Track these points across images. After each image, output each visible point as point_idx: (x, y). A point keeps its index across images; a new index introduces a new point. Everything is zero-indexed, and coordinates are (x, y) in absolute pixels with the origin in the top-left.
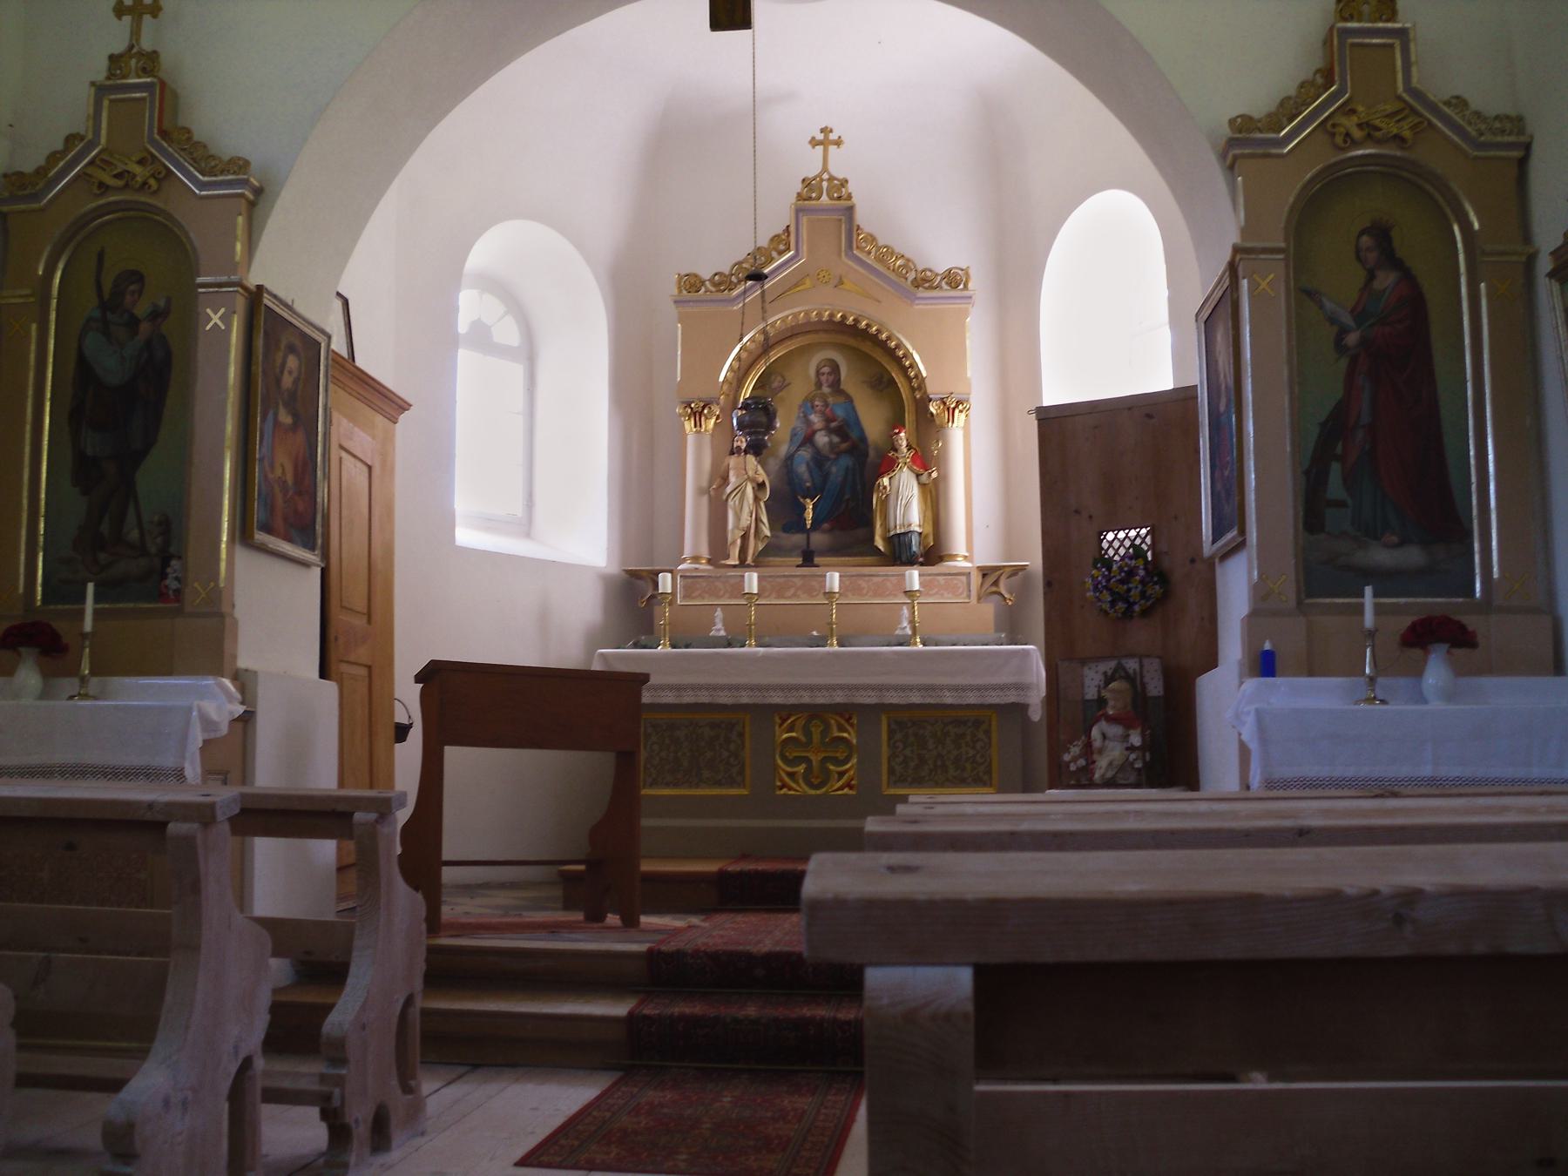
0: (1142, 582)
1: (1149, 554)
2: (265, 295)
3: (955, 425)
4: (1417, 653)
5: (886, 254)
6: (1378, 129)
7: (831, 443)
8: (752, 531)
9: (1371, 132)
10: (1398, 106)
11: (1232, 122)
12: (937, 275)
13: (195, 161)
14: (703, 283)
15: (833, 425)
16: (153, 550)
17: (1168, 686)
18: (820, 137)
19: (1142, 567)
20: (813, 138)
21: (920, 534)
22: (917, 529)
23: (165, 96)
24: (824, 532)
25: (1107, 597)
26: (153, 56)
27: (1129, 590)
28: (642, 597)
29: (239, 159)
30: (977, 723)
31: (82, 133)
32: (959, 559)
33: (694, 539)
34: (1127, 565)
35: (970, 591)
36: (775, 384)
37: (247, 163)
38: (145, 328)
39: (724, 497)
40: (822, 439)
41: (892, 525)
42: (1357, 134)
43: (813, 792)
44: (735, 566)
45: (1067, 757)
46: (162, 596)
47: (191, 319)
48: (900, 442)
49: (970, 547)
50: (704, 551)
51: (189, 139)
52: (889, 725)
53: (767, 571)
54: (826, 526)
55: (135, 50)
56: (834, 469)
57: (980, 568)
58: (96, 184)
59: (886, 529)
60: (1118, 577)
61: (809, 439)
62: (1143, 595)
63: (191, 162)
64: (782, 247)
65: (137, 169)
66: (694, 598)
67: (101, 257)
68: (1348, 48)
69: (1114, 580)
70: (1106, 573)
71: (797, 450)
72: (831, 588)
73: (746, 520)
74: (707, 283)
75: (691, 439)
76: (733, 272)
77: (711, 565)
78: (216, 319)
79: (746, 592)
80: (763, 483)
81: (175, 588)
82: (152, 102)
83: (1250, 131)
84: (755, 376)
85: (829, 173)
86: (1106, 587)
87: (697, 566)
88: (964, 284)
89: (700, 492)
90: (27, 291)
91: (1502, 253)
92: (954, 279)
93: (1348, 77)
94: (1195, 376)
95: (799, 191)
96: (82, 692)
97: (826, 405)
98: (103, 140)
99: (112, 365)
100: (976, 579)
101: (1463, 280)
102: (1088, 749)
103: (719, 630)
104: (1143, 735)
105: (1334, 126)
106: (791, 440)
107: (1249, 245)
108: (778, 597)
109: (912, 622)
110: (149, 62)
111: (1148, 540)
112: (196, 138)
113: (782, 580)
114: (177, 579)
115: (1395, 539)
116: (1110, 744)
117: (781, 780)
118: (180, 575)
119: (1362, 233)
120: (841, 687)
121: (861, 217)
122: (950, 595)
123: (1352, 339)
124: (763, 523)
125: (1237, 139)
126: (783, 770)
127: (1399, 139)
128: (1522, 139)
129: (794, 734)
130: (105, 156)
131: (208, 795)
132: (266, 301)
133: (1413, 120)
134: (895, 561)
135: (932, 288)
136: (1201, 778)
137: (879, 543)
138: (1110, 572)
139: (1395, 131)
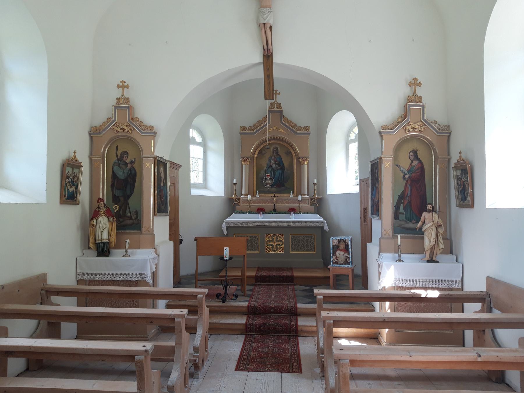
5: (290, 122)
7: (276, 166)
9: (414, 129)
12: (302, 128)
14: (246, 129)
15: (277, 163)
16: (134, 218)
24: (275, 188)
36: (263, 153)
38: (129, 166)
40: (274, 166)
43: (274, 252)
47: (141, 166)
49: (308, 193)
51: (138, 121)
52: (291, 237)
56: (277, 173)
63: (139, 126)
67: (117, 147)
78: (148, 165)
85: (277, 102)
90: (100, 156)
97: (275, 158)
101: (433, 163)
105: (406, 128)
112: (140, 120)
117: (267, 249)
119: (410, 152)
121: (284, 113)
123: (407, 176)
128: (449, 131)
130: (117, 124)
131: (181, 311)
139: (420, 129)
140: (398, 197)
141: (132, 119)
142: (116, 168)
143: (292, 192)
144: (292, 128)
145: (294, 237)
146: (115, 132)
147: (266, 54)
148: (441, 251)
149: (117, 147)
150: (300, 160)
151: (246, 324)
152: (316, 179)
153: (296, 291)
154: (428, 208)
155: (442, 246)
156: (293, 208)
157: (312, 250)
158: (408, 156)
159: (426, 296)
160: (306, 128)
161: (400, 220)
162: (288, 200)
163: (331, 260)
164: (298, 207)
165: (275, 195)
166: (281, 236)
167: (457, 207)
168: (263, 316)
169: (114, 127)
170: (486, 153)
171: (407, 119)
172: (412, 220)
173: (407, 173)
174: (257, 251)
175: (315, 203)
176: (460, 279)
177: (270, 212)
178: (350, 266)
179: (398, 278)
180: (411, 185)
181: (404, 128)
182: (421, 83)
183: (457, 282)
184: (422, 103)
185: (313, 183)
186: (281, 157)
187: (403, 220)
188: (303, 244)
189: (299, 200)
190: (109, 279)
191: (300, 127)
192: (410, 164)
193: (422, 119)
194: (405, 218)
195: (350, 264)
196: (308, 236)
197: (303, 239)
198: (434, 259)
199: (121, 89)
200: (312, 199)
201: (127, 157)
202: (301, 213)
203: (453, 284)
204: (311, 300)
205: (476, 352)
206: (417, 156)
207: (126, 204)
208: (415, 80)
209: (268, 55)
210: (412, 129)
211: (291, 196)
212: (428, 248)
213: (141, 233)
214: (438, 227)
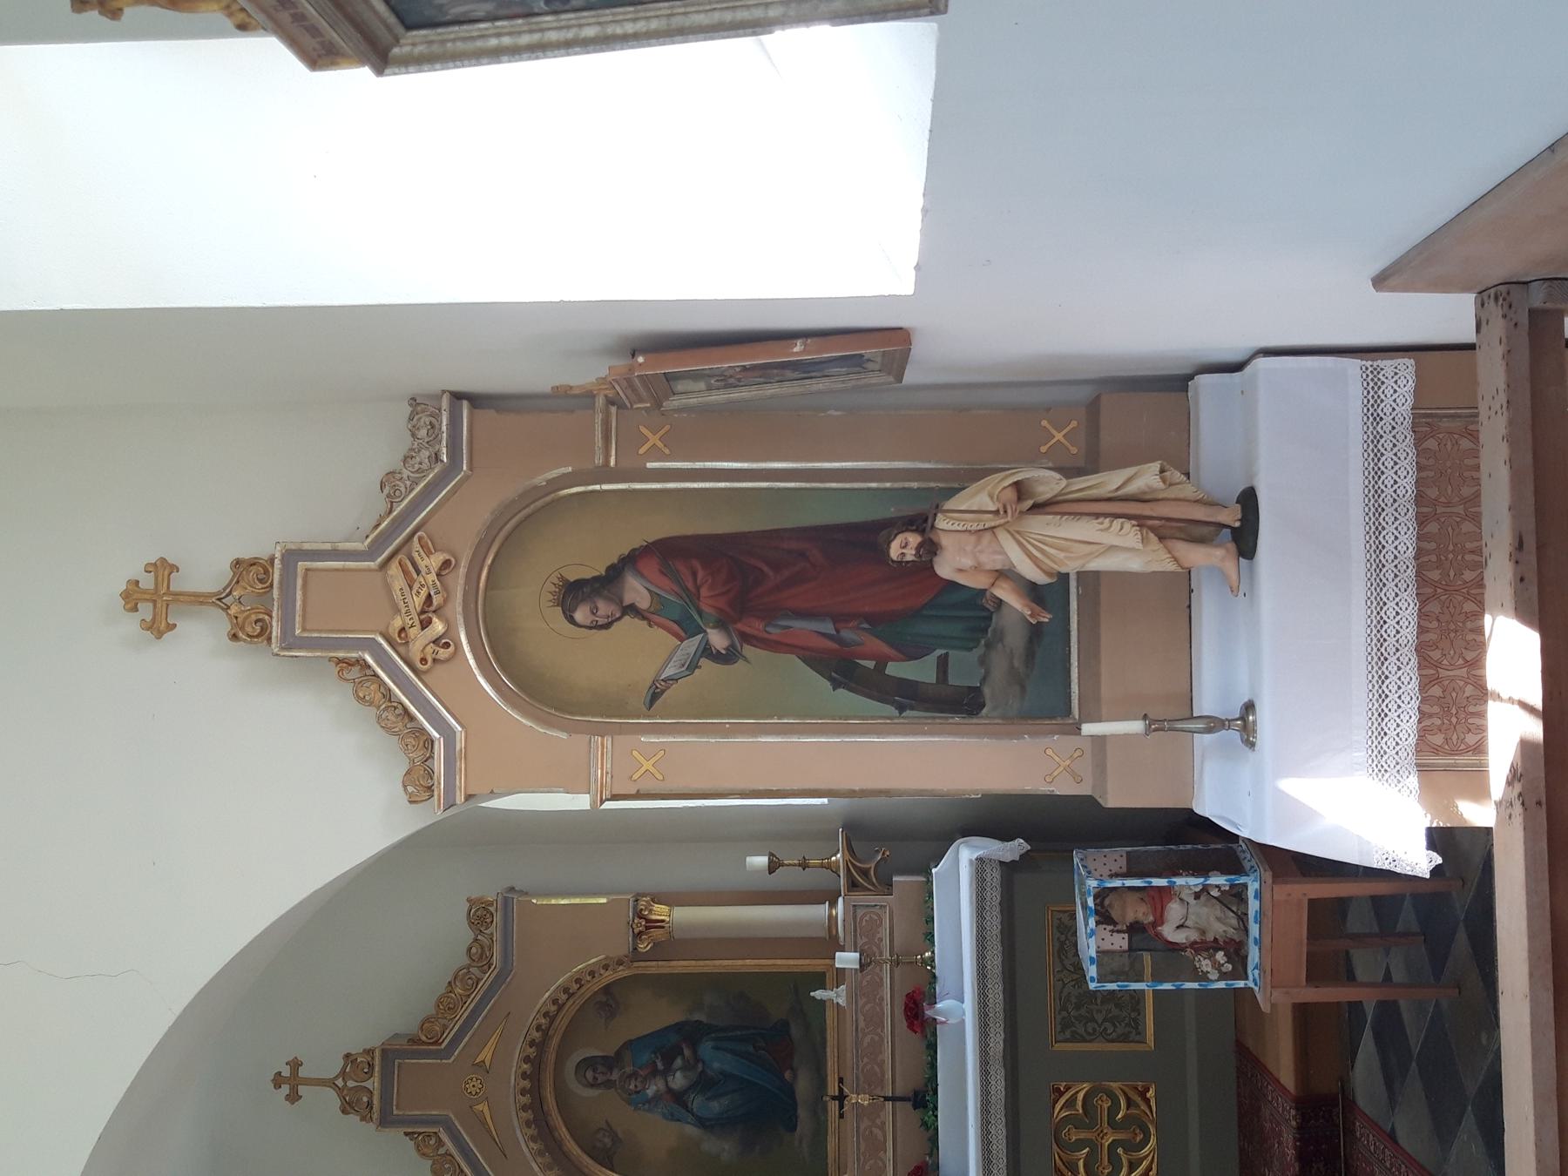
3: (667, 919)
5: (446, 1005)
7: (684, 1069)
12: (476, 940)
15: (660, 1066)
18: (285, 1089)
20: (288, 1098)
24: (795, 1076)
40: (678, 1081)
43: (1153, 1141)
52: (1066, 1041)
54: (787, 1075)
56: (716, 1065)
71: (690, 1111)
85: (336, 1077)
95: (358, 1118)
97: (634, 1075)
105: (424, 660)
106: (679, 1120)
119: (572, 620)
123: (718, 640)
139: (432, 577)
140: (841, 690)
143: (818, 994)
144: (476, 997)
145: (1065, 1025)
148: (1178, 476)
152: (749, 859)
154: (909, 558)
155: (1147, 478)
156: (907, 1008)
158: (594, 631)
159: (1530, 709)
160: (479, 915)
161: (984, 680)
162: (861, 1018)
163: (1221, 985)
164: (897, 971)
165: (834, 1098)
166: (1062, 1101)
170: (557, 299)
171: (373, 656)
172: (984, 609)
173: (700, 636)
175: (873, 865)
176: (1352, 365)
177: (928, 1129)
178: (1256, 885)
179: (1361, 755)
180: (770, 614)
182: (155, 565)
183: (1378, 384)
184: (272, 560)
185: (770, 873)
186: (631, 1042)
187: (983, 661)
189: (858, 967)
190: (1407, 445)
191: (474, 950)
192: (645, 622)
194: (970, 649)
195: (1245, 886)
196: (1057, 945)
198: (1231, 516)
200: (853, 885)
202: (932, 959)
203: (1388, 410)
206: (595, 579)
208: (132, 597)
210: (430, 622)
211: (836, 996)
212: (1164, 555)
214: (1024, 498)
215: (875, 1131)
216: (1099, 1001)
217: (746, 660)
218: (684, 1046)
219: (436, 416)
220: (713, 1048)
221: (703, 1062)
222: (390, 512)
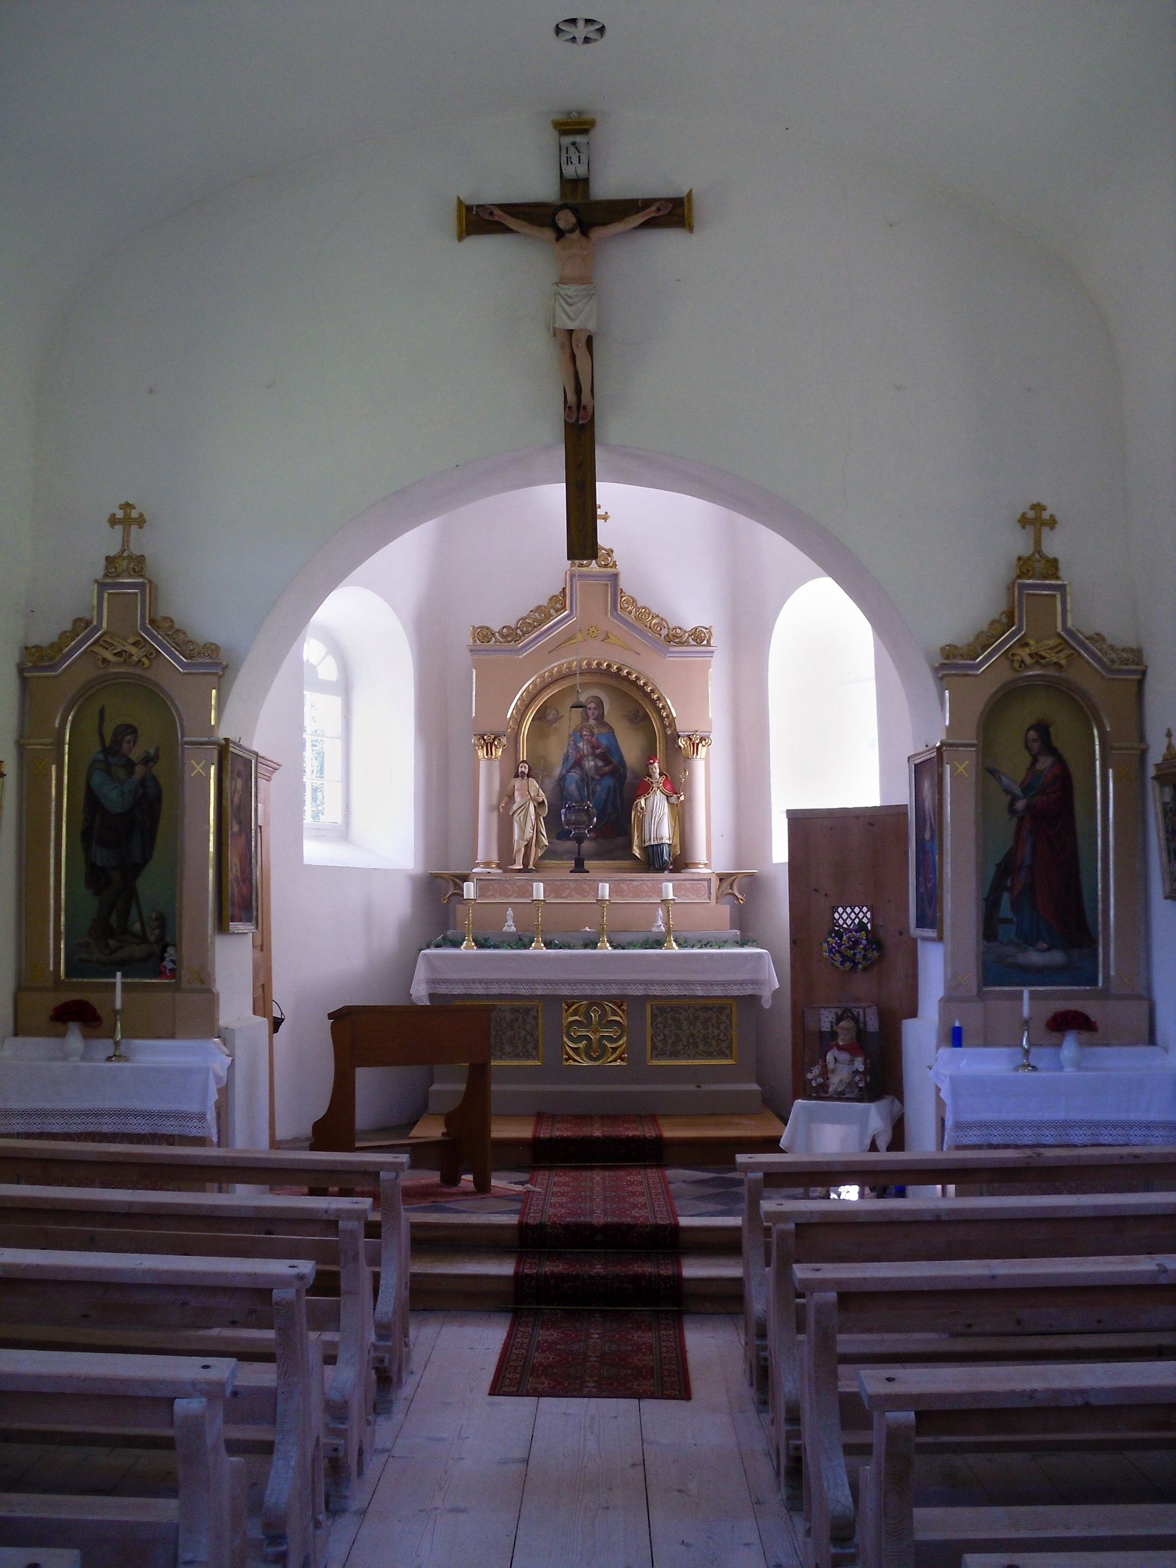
0: (865, 949)
1: (869, 925)
2: (231, 745)
3: (698, 757)
4: (1057, 1035)
6: (1044, 658)
7: (596, 766)
8: (534, 841)
9: (1037, 657)
10: (1058, 641)
11: (942, 649)
12: (685, 632)
13: (177, 645)
14: (493, 635)
15: (598, 751)
16: (152, 938)
17: (881, 1022)
19: (864, 938)
21: (669, 845)
22: (668, 842)
23: (149, 589)
25: (838, 957)
26: (141, 559)
27: (855, 954)
28: (444, 895)
29: (212, 644)
30: (722, 1009)
31: (88, 617)
32: (700, 866)
33: (486, 848)
34: (854, 936)
35: (710, 894)
36: (550, 717)
37: (217, 648)
38: (139, 770)
39: (511, 814)
41: (647, 837)
42: (1028, 660)
44: (519, 871)
45: (809, 1076)
46: (160, 974)
48: (654, 770)
49: (709, 857)
50: (494, 857)
51: (171, 627)
53: (550, 875)
55: (125, 554)
56: (598, 788)
57: (718, 875)
58: (100, 660)
59: (642, 841)
60: (847, 945)
61: (578, 764)
62: (865, 957)
63: (175, 645)
64: (558, 606)
65: (133, 650)
66: (487, 897)
67: (102, 713)
68: (1024, 597)
69: (844, 946)
70: (839, 941)
71: (568, 772)
72: (603, 896)
73: (529, 832)
74: (497, 634)
75: (483, 765)
76: (519, 626)
77: (500, 869)
79: (534, 899)
80: (543, 801)
81: (170, 968)
82: (143, 596)
83: (955, 657)
84: (532, 713)
86: (838, 952)
87: (489, 870)
88: (707, 640)
89: (491, 808)
91: (1127, 749)
92: (699, 637)
93: (1024, 619)
94: (903, 796)
96: (116, 1054)
97: (592, 734)
98: (105, 625)
99: (114, 798)
100: (715, 883)
102: (825, 1073)
103: (510, 927)
104: (865, 1064)
105: (1013, 655)
107: (951, 741)
108: (555, 898)
109: (667, 924)
110: (138, 564)
111: (869, 915)
112: (177, 626)
113: (559, 883)
114: (172, 961)
115: (1045, 946)
116: (840, 1066)
117: (567, 1054)
118: (174, 959)
119: (1030, 729)
120: (616, 982)
121: (623, 583)
122: (695, 897)
123: (1020, 805)
124: (543, 835)
125: (946, 664)
126: (568, 1046)
127: (1058, 665)
128: (1141, 668)
129: (577, 1018)
132: (231, 749)
133: (1067, 652)
134: (649, 867)
135: (681, 644)
136: (905, 1090)
137: (637, 852)
138: (841, 941)
139: (1055, 660)
141: (152, 622)
142: (98, 778)
146: (100, 663)
147: (573, 420)
149: (102, 713)
150: (681, 743)
151: (517, 1277)
153: (670, 1185)
157: (722, 1055)
167: (1166, 898)
168: (568, 1256)
169: (96, 649)
173: (1022, 795)
174: (534, 1058)
181: (1009, 655)
184: (1058, 578)
186: (613, 732)
188: (692, 1035)
193: (1059, 629)
197: (691, 1016)
199: (122, 529)
201: (132, 743)
204: (720, 1207)
205: (1158, 1262)
207: (130, 893)
209: (581, 422)
213: (177, 988)
215: (568, 891)
216: (676, 1031)
217: (1010, 819)
218: (610, 767)
219: (1133, 663)
220: (609, 787)
221: (599, 780)
222: (1087, 638)
